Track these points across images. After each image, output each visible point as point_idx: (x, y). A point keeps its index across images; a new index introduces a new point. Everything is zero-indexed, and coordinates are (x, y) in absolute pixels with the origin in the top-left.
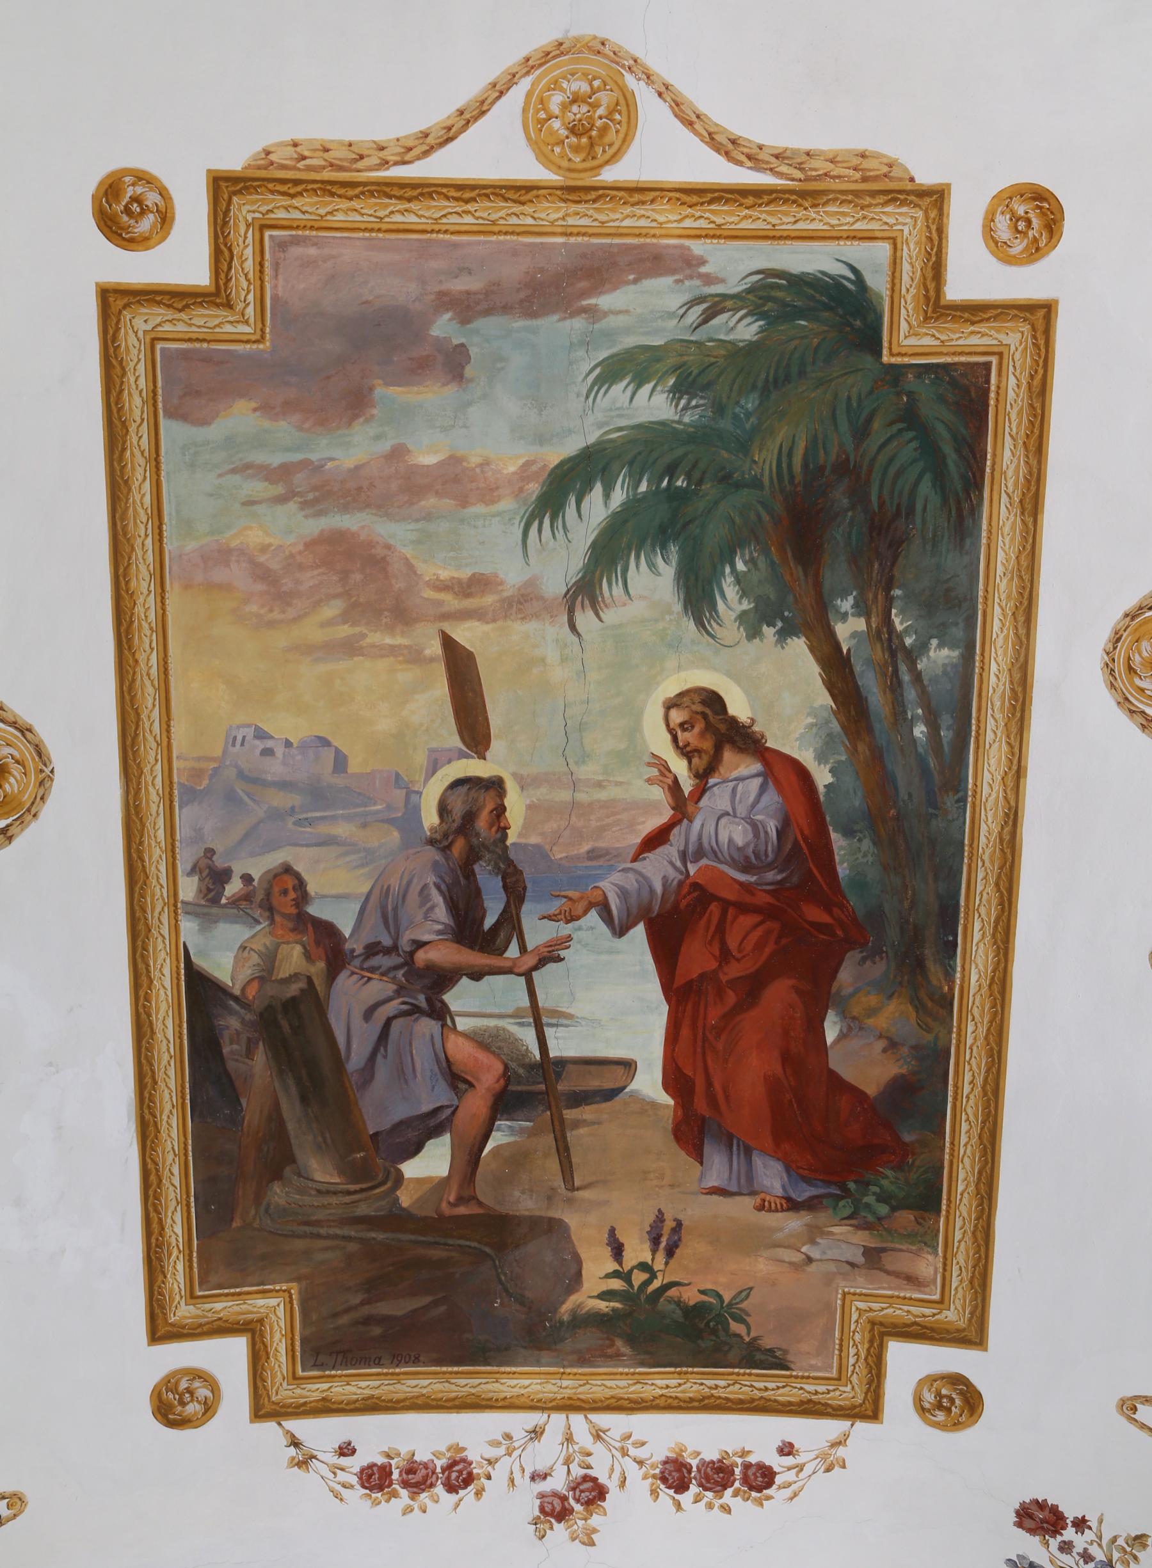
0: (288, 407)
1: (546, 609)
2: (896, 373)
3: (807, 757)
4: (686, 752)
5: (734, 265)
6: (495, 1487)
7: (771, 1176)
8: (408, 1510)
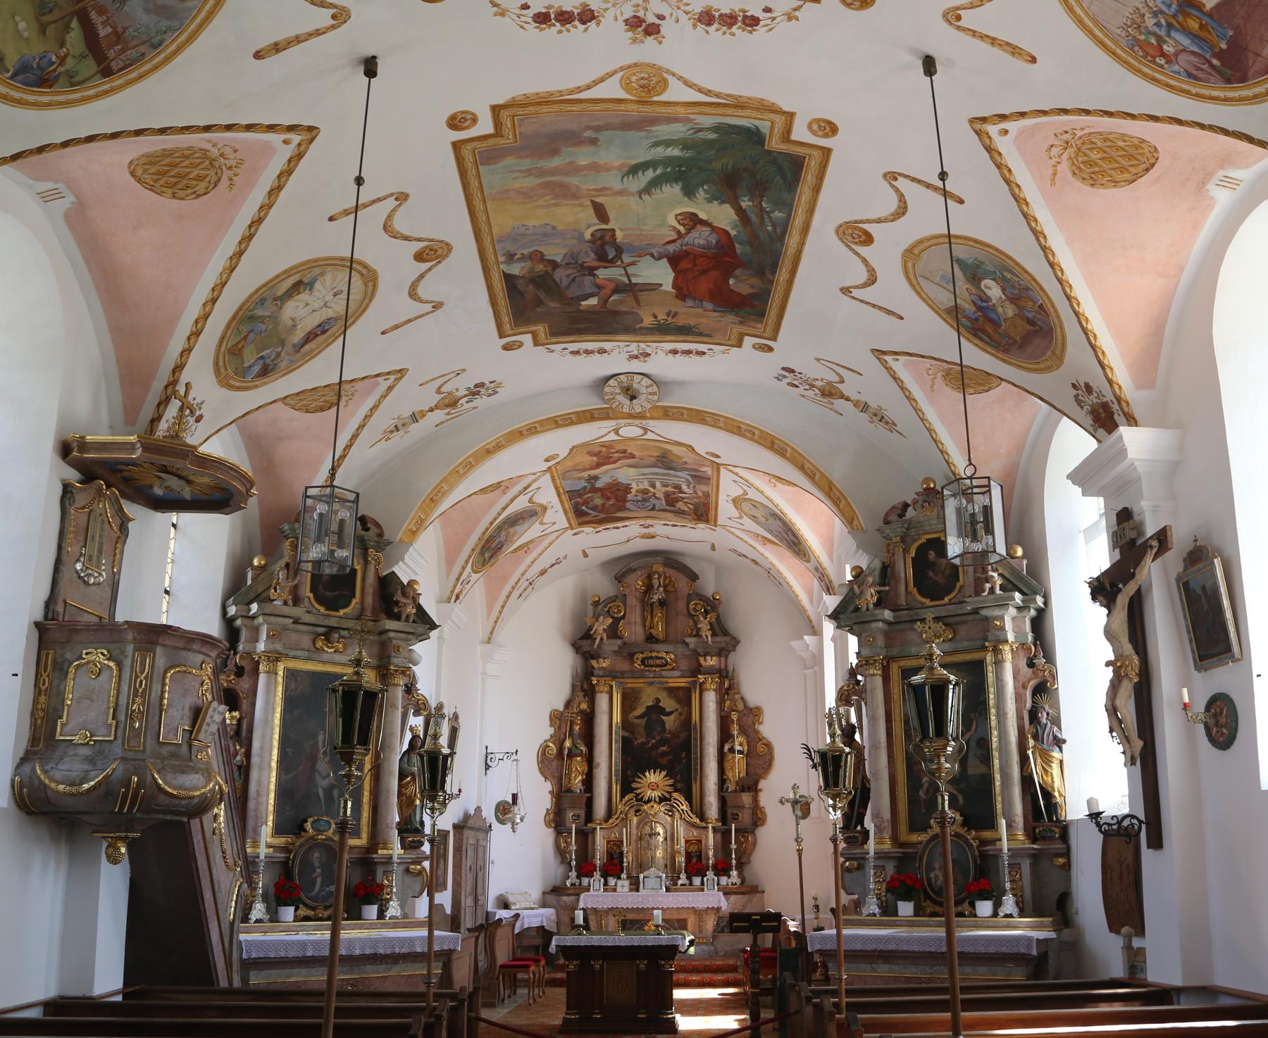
0: (527, 156)
1: (632, 194)
2: (770, 152)
3: (728, 228)
5: (709, 121)
6: (607, 20)
7: (709, 306)
8: (560, 32)
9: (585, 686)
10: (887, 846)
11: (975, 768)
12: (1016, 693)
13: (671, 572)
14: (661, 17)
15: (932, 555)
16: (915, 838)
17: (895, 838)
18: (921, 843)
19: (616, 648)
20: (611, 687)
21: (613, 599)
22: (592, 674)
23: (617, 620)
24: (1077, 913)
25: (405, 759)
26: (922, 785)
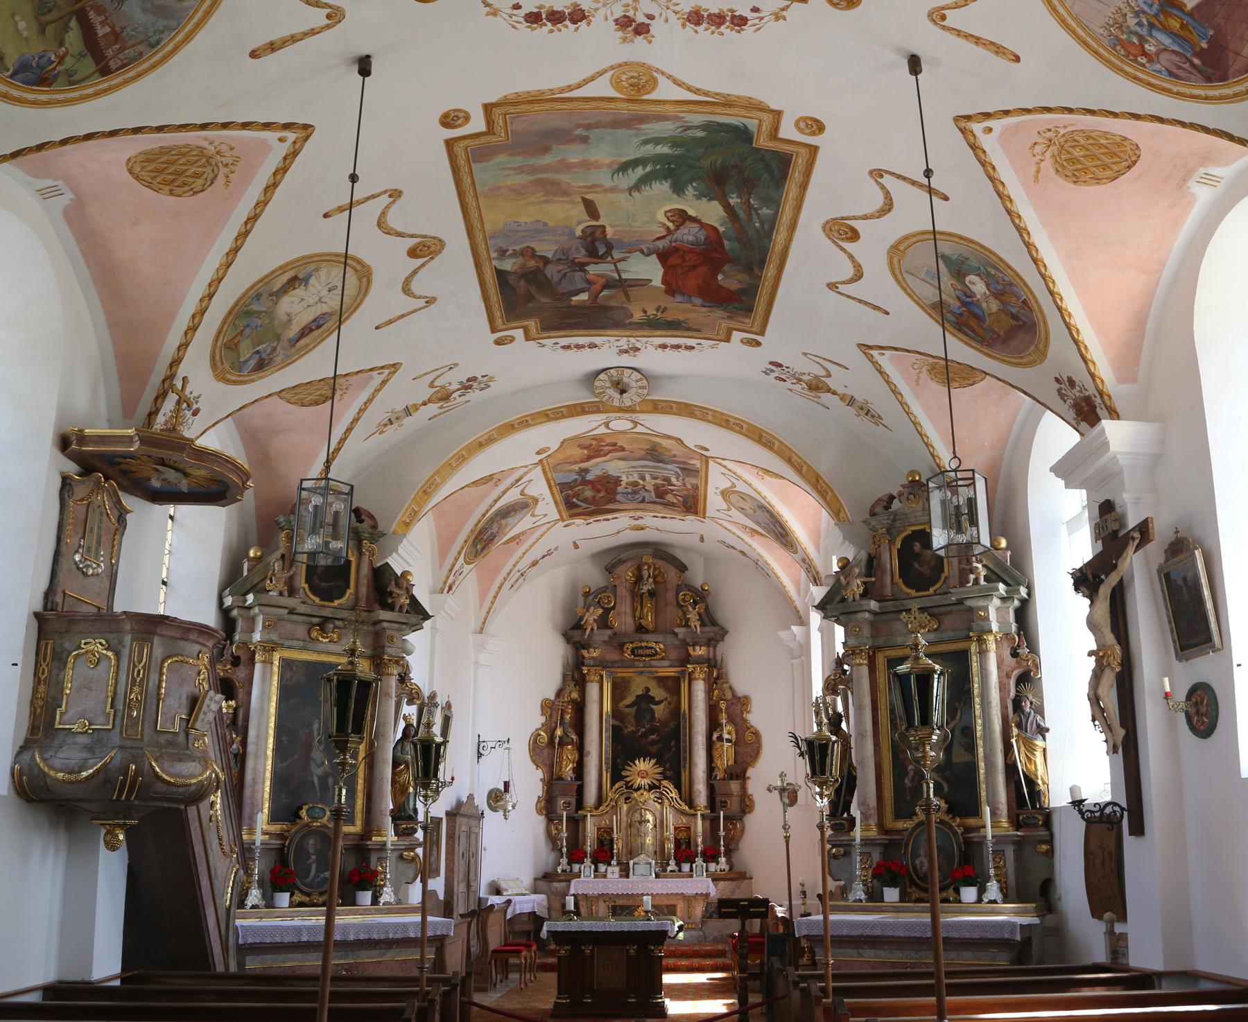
0: (519, 154)
1: (622, 191)
2: (758, 150)
3: (717, 225)
4: (673, 221)
5: (698, 119)
6: (598, 19)
7: (698, 301)
8: (551, 31)
9: (576, 675)
10: (873, 833)
11: (959, 756)
12: (1000, 683)
13: (660, 563)
14: (651, 17)
15: (917, 546)
16: (901, 825)
17: (881, 825)
18: (906, 830)
19: (606, 638)
20: (602, 676)
21: (603, 590)
22: (583, 664)
23: (607, 611)
24: (1060, 899)
25: (399, 748)
26: (907, 773)
